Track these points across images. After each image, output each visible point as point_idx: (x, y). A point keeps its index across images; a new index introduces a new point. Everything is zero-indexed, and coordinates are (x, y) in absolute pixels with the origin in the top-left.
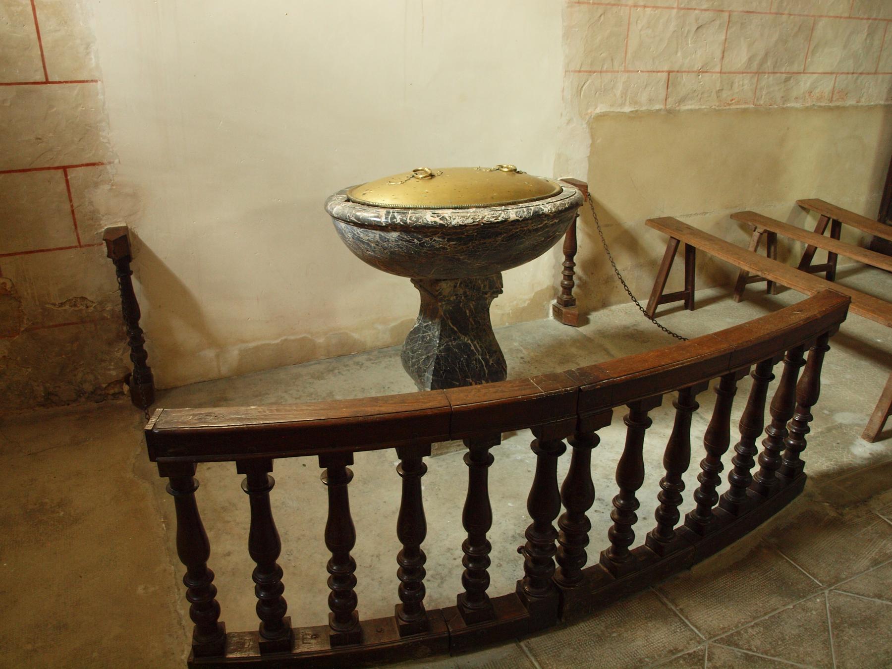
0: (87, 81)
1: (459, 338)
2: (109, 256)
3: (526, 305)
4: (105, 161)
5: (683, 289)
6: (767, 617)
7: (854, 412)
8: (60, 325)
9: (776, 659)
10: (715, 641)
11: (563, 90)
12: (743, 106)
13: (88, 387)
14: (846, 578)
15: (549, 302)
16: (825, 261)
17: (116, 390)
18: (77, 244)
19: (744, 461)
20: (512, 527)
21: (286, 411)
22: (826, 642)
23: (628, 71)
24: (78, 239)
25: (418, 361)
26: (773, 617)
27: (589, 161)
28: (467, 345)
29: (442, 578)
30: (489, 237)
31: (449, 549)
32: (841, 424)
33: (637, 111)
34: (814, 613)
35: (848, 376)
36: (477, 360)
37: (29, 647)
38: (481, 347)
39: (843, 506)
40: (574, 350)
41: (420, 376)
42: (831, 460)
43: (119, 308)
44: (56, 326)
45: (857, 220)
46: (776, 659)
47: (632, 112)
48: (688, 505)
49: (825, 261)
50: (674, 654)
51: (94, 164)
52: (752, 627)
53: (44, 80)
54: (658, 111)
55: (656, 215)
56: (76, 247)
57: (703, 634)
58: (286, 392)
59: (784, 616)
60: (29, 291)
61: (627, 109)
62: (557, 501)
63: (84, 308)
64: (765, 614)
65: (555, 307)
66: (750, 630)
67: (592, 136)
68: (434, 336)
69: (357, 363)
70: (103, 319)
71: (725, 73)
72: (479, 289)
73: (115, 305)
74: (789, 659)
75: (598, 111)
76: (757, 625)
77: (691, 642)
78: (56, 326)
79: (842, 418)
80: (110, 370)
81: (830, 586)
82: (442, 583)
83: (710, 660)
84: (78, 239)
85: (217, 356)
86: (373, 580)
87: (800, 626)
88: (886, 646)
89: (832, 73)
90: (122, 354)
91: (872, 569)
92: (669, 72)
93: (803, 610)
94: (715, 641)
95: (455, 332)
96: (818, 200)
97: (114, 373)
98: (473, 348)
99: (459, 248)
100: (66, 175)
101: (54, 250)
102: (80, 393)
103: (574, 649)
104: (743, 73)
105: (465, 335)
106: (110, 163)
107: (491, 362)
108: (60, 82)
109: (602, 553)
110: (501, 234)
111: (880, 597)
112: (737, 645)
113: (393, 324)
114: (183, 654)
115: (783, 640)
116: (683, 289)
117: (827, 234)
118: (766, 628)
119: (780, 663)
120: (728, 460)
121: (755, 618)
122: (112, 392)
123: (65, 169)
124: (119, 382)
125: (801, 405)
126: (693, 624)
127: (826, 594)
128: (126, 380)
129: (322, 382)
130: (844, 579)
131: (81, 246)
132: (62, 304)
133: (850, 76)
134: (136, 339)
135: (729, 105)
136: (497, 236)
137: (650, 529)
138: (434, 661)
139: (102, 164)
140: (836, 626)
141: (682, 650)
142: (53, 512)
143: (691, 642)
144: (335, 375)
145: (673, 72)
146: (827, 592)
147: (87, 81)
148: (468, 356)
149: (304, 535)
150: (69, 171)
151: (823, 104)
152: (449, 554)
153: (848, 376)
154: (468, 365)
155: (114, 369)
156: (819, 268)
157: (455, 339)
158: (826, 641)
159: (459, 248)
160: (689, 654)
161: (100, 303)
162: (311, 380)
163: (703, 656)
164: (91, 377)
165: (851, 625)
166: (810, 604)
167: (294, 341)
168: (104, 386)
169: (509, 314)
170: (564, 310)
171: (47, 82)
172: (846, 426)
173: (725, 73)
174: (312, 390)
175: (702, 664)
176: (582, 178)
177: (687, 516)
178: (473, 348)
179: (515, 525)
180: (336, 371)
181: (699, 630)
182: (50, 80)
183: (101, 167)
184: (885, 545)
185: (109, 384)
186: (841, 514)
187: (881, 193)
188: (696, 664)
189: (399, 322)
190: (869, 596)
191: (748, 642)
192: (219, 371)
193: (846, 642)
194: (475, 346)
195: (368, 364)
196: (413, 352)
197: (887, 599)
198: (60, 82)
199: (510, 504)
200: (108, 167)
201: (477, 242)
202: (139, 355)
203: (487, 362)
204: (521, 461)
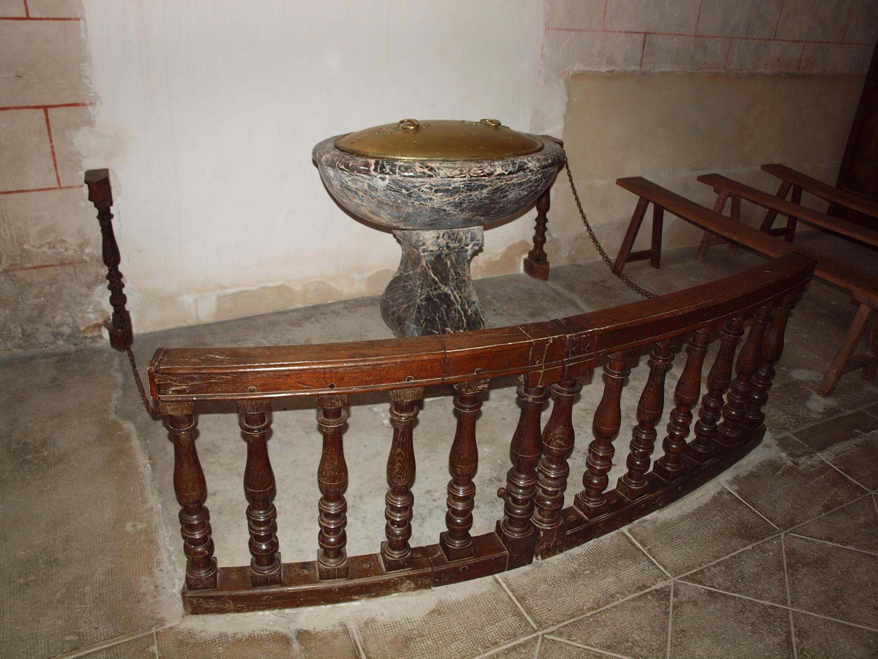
0: (69, 19)
1: (439, 288)
2: (90, 199)
3: (498, 258)
4: (87, 102)
5: (649, 248)
6: (727, 557)
7: (810, 369)
8: (38, 267)
9: (736, 595)
10: (680, 579)
11: (542, 48)
12: (714, 71)
13: (66, 330)
14: (801, 522)
15: (520, 256)
16: (784, 225)
17: (95, 334)
18: (57, 186)
19: (679, 425)
20: (489, 471)
21: (171, 380)
22: (781, 580)
23: (607, 31)
24: (58, 180)
25: (399, 310)
26: (734, 556)
27: (565, 119)
28: (447, 295)
29: (423, 518)
30: (476, 190)
31: (429, 492)
32: (797, 380)
33: (613, 71)
34: (771, 553)
35: (804, 336)
36: (456, 310)
37: (22, 581)
38: (460, 297)
39: (800, 456)
40: (545, 304)
41: (400, 324)
42: (788, 414)
43: (99, 252)
44: (35, 268)
45: (815, 186)
46: (736, 595)
47: (608, 72)
48: (618, 472)
49: (784, 225)
50: (642, 590)
51: (75, 105)
52: (715, 566)
53: (25, 16)
54: (633, 71)
55: (628, 174)
56: (55, 188)
57: (670, 572)
58: (264, 338)
59: (744, 556)
60: (8, 232)
61: (603, 69)
62: (535, 448)
63: (62, 250)
64: (727, 554)
65: (526, 262)
66: (713, 569)
67: (569, 94)
68: (415, 285)
69: (334, 312)
70: (83, 262)
71: (699, 36)
72: (460, 241)
73: (96, 248)
74: (748, 595)
75: (576, 69)
76: (719, 564)
77: (658, 580)
78: (35, 268)
79: (800, 375)
80: (88, 313)
81: (785, 529)
82: (423, 523)
83: (675, 596)
84: (58, 180)
85: (196, 301)
86: (356, 519)
87: (758, 566)
88: (835, 584)
89: (801, 42)
90: (102, 296)
91: (823, 514)
92: (646, 34)
93: (762, 551)
94: (680, 579)
95: (436, 283)
96: (640, 178)
97: (92, 316)
98: (452, 298)
99: (446, 199)
100: (46, 115)
101: (33, 190)
102: (57, 335)
103: (550, 585)
104: (716, 37)
105: (446, 285)
106: (91, 104)
107: (469, 312)
108: (41, 19)
109: (576, 496)
110: (486, 187)
111: (831, 540)
112: (700, 583)
113: (369, 274)
114: (174, 588)
115: (743, 578)
116: (649, 248)
117: (789, 198)
118: (727, 567)
119: (740, 599)
120: (622, 446)
121: (717, 558)
122: (90, 335)
123: (45, 108)
124: (98, 326)
125: (740, 372)
126: (660, 563)
127: (783, 537)
128: (106, 324)
129: (299, 329)
130: (798, 523)
131: (61, 188)
132: (41, 246)
133: (818, 45)
134: (116, 282)
135: (702, 69)
136: (482, 189)
137: (622, 475)
138: (418, 594)
139: (83, 105)
140: (790, 565)
141: (650, 587)
142: (37, 452)
143: (658, 580)
144: (312, 323)
145: (649, 33)
146: (782, 535)
147: (69, 19)
148: (448, 306)
149: (287, 476)
150: (50, 110)
151: (791, 72)
152: (429, 496)
153: (804, 336)
154: (447, 315)
155: (92, 313)
156: (777, 232)
157: (435, 289)
158: (781, 579)
159: (446, 199)
160: (657, 591)
161: (80, 246)
162: (289, 327)
163: (669, 592)
164: (70, 321)
165: (804, 566)
166: (767, 546)
167: (271, 288)
168: (82, 329)
169: (481, 267)
170: (535, 265)
171: (28, 18)
172: (802, 382)
173: (699, 36)
174: (290, 337)
175: (668, 600)
176: (559, 137)
177: (656, 462)
178: (452, 298)
179: (491, 469)
180: (313, 319)
181: (666, 569)
182: (31, 16)
183: (82, 108)
184: (836, 493)
185: (88, 328)
186: (797, 464)
187: (840, 161)
188: (662, 599)
189: (375, 271)
190: (821, 539)
191: (711, 580)
192: (197, 316)
193: (800, 581)
194: (454, 296)
195: (345, 312)
196: (394, 301)
197: (838, 542)
198: (41, 19)
199: (486, 450)
200: (90, 108)
201: (464, 194)
202: (118, 299)
203: (465, 312)
204: (496, 408)
